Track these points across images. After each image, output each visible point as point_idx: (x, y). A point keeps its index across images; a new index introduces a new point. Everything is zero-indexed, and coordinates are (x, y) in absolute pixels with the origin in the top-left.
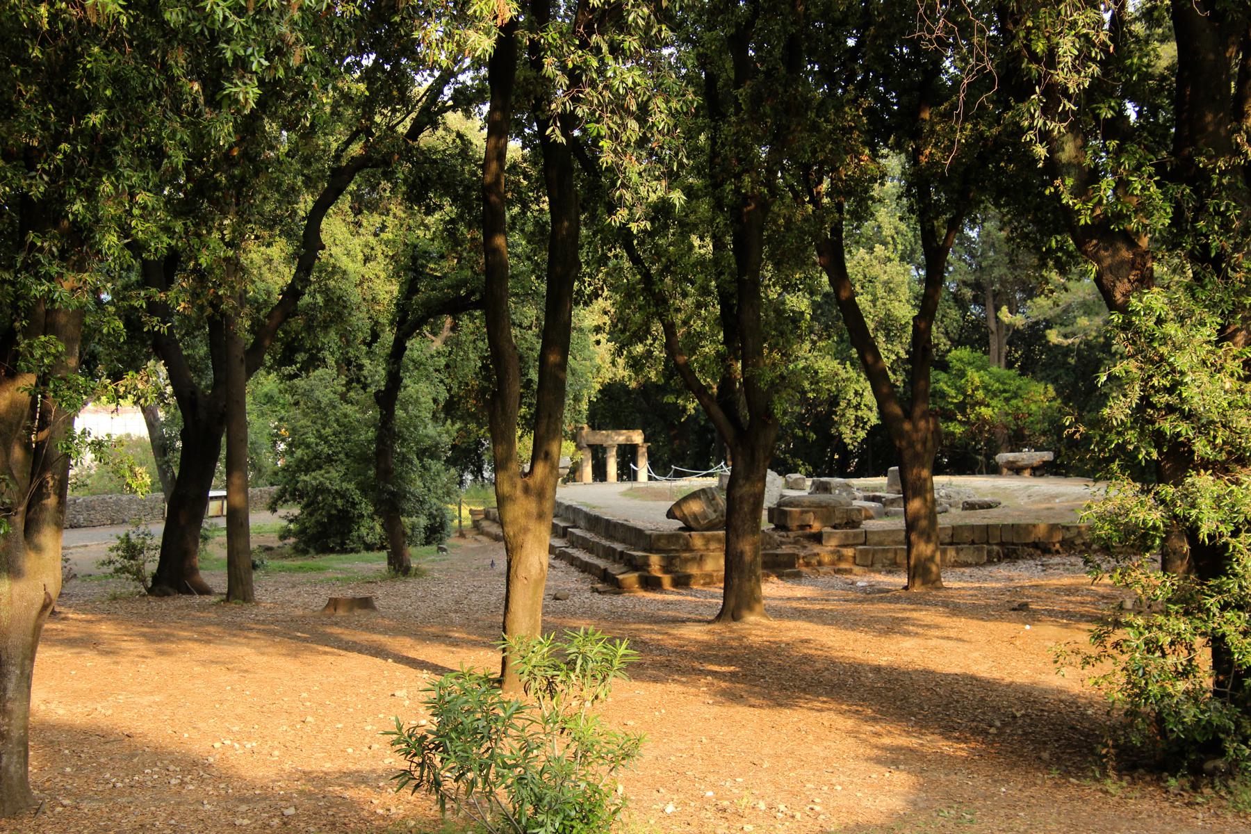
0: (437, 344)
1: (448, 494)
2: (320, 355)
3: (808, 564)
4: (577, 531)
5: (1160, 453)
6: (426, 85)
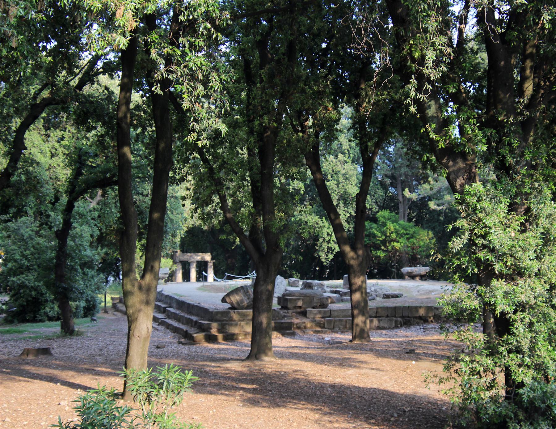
0: (93, 204)
1: (98, 289)
2: (24, 209)
3: (299, 328)
4: (172, 310)
5: (479, 270)
6: (87, 60)
